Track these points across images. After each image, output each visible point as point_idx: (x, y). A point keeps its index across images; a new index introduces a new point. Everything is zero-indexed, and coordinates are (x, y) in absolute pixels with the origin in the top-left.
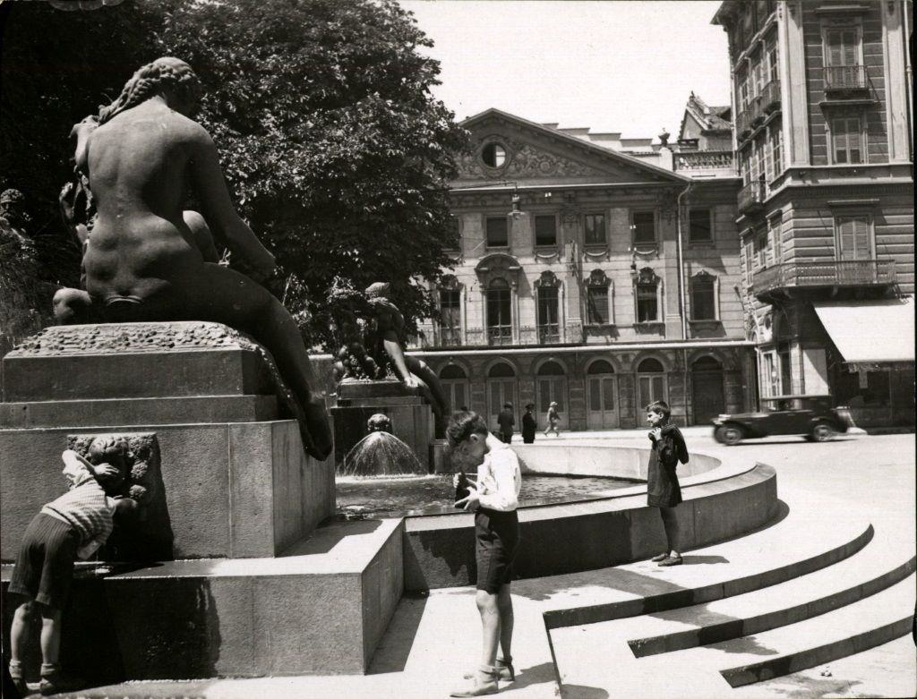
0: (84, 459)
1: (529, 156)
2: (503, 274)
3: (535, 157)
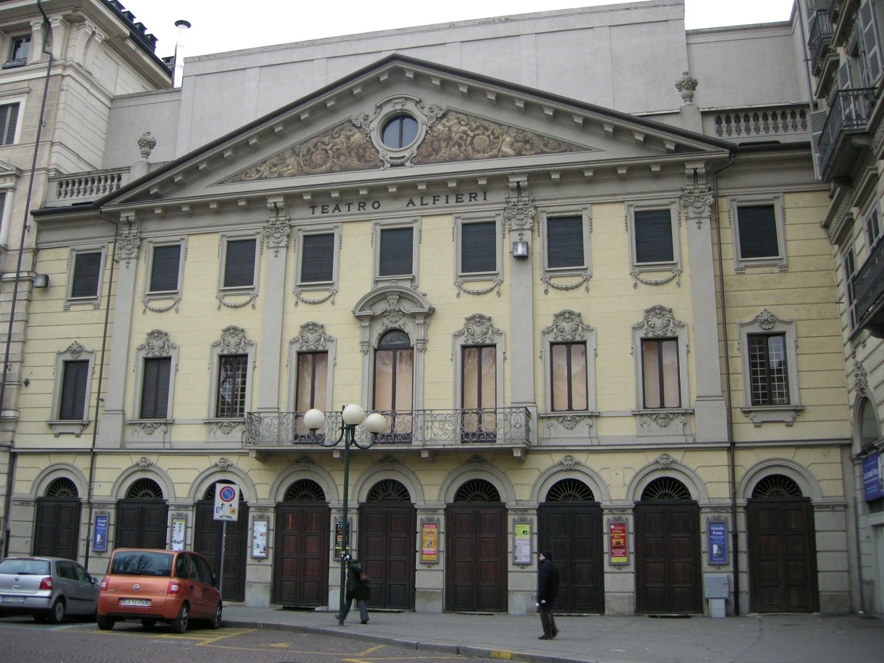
0: (848, 208)
1: (454, 129)
2: (401, 323)
3: (465, 128)
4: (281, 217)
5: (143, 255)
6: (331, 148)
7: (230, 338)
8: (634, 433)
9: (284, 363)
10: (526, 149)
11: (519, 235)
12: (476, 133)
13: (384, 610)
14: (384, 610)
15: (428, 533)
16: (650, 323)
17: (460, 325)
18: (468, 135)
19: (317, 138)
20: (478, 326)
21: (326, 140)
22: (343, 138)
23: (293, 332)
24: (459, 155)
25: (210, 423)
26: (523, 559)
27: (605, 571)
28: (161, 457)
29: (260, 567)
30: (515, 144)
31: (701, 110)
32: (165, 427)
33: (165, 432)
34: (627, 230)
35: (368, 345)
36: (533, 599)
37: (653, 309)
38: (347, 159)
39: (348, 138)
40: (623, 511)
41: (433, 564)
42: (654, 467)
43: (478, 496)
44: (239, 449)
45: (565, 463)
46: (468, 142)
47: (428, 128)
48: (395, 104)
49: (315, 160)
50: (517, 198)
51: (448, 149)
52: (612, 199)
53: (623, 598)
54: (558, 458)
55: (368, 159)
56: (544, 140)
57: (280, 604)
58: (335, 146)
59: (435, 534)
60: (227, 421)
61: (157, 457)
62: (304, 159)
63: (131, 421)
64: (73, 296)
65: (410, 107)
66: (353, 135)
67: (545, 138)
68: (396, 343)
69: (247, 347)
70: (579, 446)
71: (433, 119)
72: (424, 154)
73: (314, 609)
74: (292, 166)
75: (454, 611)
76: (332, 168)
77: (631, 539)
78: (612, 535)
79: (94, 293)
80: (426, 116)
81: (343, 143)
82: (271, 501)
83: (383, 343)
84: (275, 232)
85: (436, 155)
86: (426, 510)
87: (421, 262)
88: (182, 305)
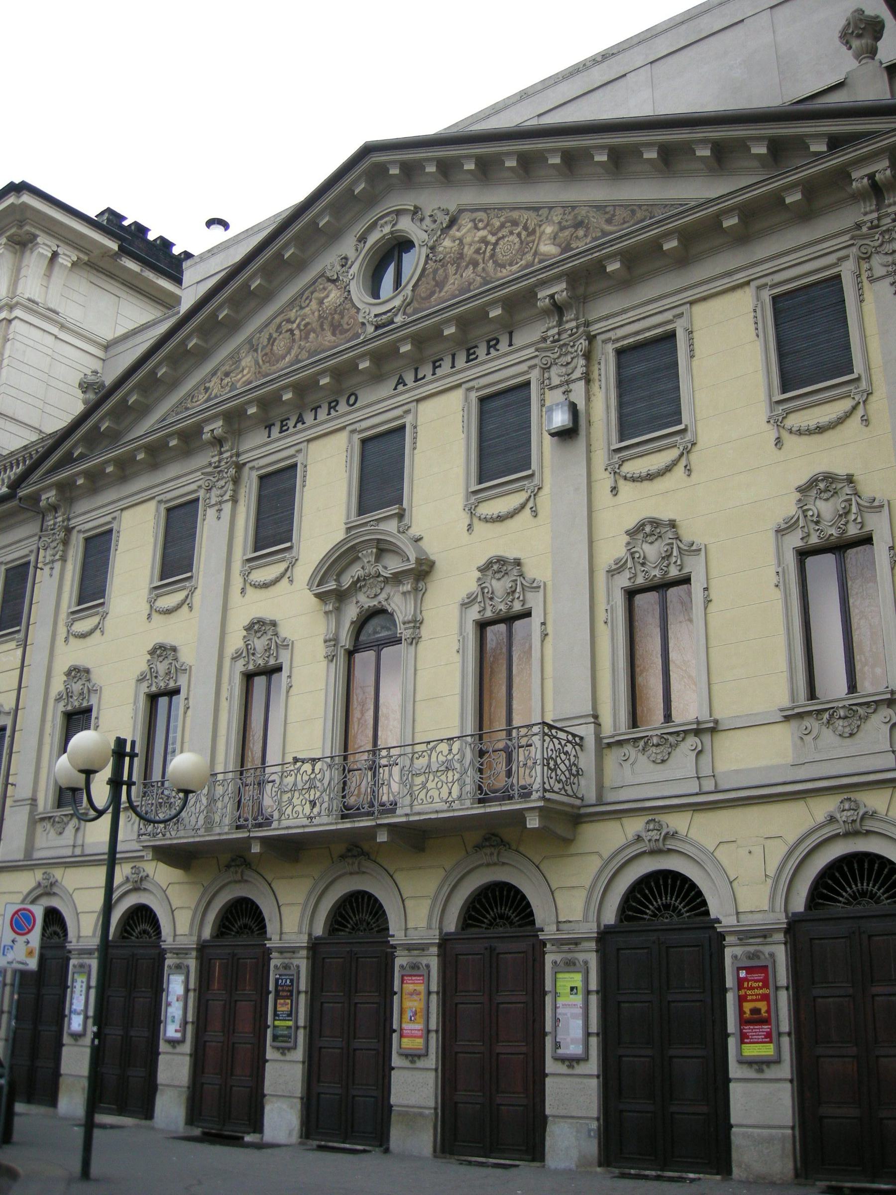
4: (567, 322)
5: (71, 553)
6: (298, 326)
7: (494, 582)
8: (790, 760)
9: (601, 616)
10: (577, 237)
11: (564, 393)
12: (500, 235)
13: (342, 1145)
14: (342, 1145)
15: (411, 994)
16: (810, 513)
17: (469, 583)
18: (487, 243)
19: (282, 316)
20: (827, 500)
21: (292, 314)
22: (314, 305)
23: (236, 641)
24: (474, 280)
25: (800, 716)
26: (572, 1047)
27: (731, 1075)
28: (67, 869)
29: (176, 1057)
30: (561, 235)
31: (884, 65)
32: (697, 739)
33: (700, 752)
34: (758, 336)
35: (334, 645)
36: (590, 1136)
37: (813, 483)
38: (318, 336)
39: (321, 302)
40: (765, 937)
41: (419, 1056)
42: (827, 832)
43: (501, 917)
44: (19, 861)
45: (646, 836)
46: (488, 254)
47: (429, 251)
48: (382, 226)
49: (276, 352)
50: (878, 210)
51: (458, 276)
52: (726, 282)
53: (770, 1140)
54: (635, 826)
55: (346, 327)
56: (606, 213)
57: (198, 1127)
58: (303, 320)
59: (423, 996)
60: (59, 814)
61: (689, 814)
62: (263, 353)
63: (612, 737)
64: (480, 482)
65: (406, 225)
66: (327, 296)
67: (608, 209)
68: (381, 635)
69: (685, 558)
70: (127, 852)
71: (436, 234)
72: (422, 295)
73: (243, 1138)
74: (247, 369)
75: (452, 1153)
76: (297, 356)
77: (784, 999)
78: (742, 992)
79: (526, 464)
80: (426, 232)
81: (313, 313)
82: (432, 932)
83: (362, 638)
84: (561, 355)
85: (440, 292)
86: (410, 948)
87: (415, 482)
88: (109, 623)
